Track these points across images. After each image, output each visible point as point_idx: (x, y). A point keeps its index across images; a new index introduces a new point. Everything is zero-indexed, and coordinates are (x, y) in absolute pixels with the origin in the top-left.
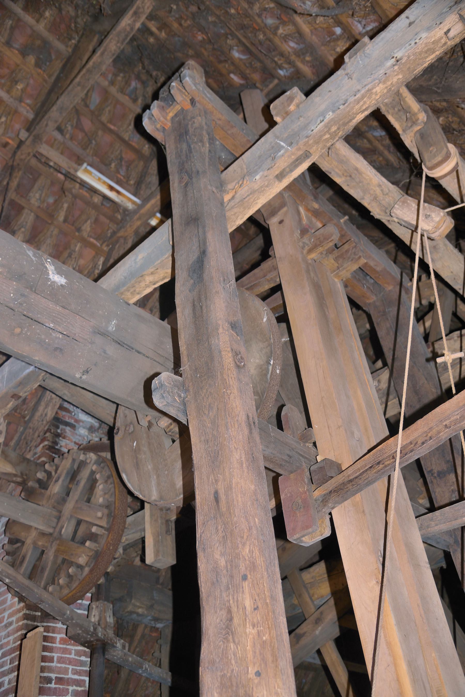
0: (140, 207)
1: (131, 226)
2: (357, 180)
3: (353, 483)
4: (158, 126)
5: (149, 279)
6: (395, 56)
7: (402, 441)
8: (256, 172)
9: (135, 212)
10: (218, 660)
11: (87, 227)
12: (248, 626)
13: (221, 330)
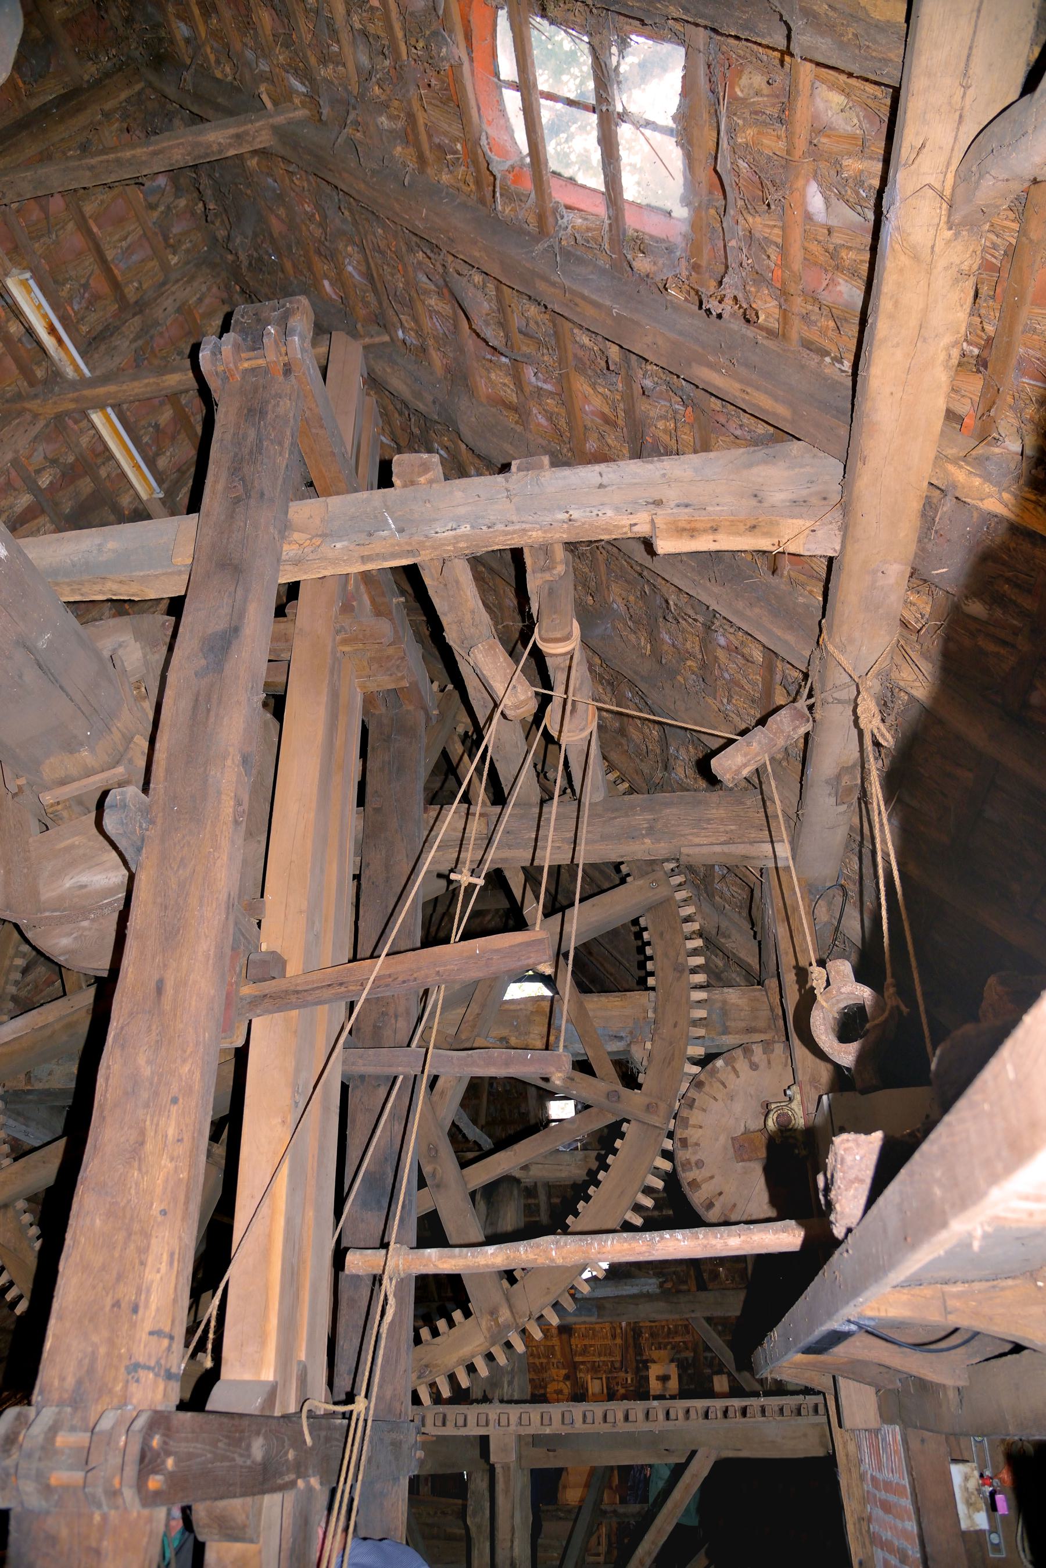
1: (55, 403)
3: (299, 996)
4: (220, 369)
5: (110, 585)
6: (571, 512)
8: (340, 538)
9: (73, 385)
10: (110, 1184)
12: (165, 1157)
13: (229, 762)
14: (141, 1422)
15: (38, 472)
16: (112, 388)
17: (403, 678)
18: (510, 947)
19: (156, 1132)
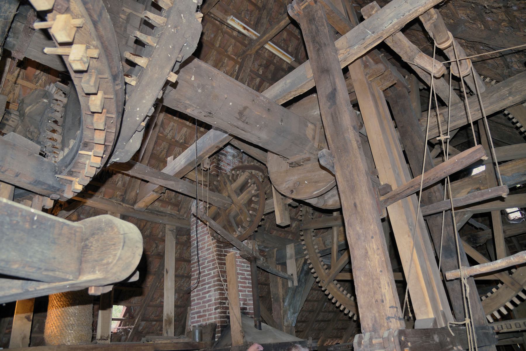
0: (259, 38)
2: (399, 44)
4: (296, 13)
8: (354, 45)
9: (257, 40)
11: (230, 49)
13: (350, 130)
14: (396, 333)
15: (258, 70)
16: (267, 35)
17: (394, 80)
18: (468, 155)
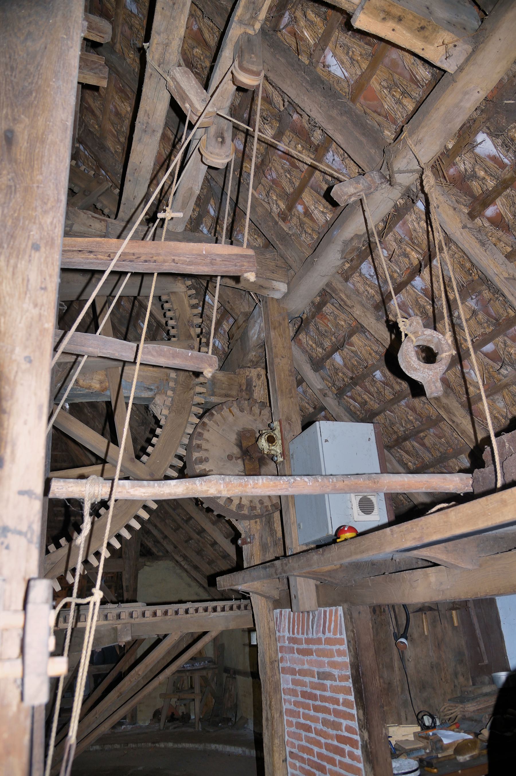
7: (125, 248)
12: (27, 300)
18: (229, 255)
19: (14, 274)
